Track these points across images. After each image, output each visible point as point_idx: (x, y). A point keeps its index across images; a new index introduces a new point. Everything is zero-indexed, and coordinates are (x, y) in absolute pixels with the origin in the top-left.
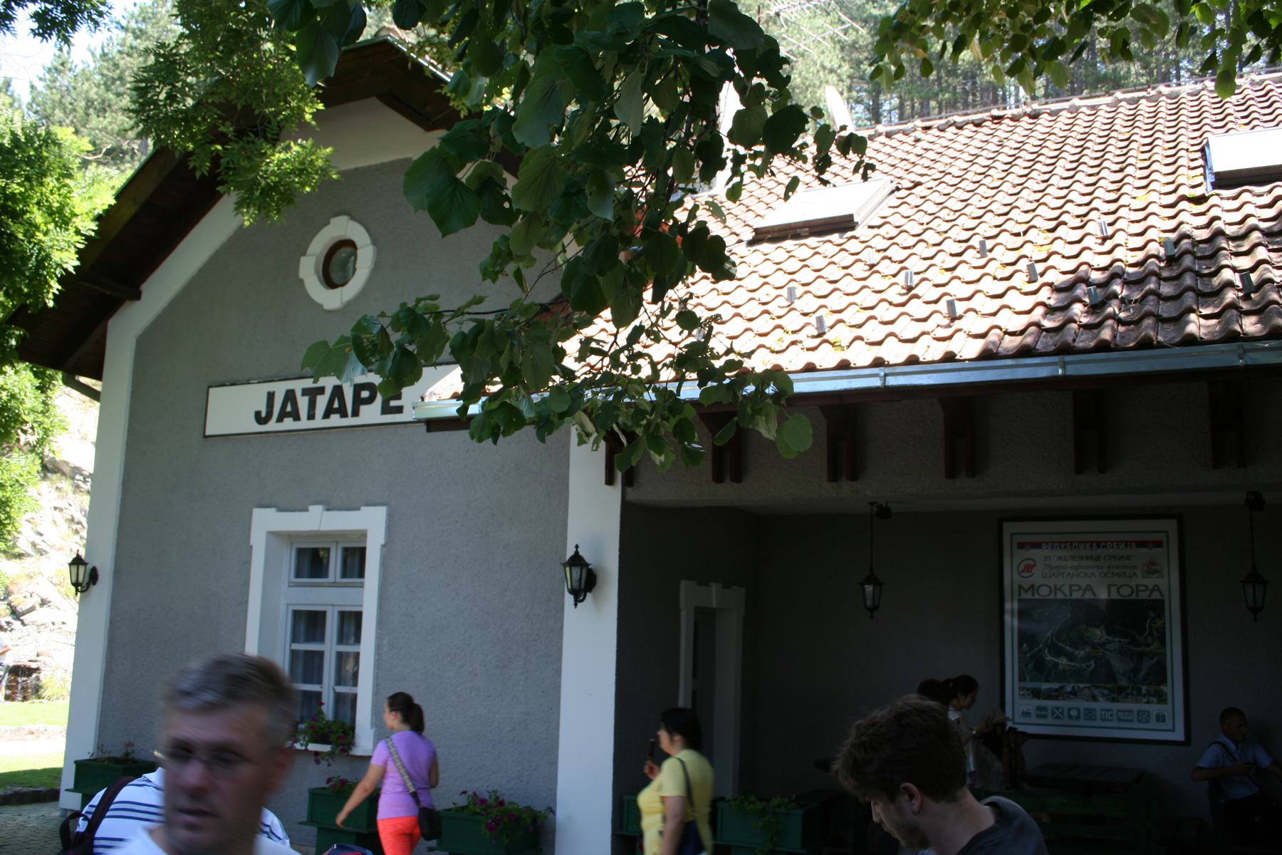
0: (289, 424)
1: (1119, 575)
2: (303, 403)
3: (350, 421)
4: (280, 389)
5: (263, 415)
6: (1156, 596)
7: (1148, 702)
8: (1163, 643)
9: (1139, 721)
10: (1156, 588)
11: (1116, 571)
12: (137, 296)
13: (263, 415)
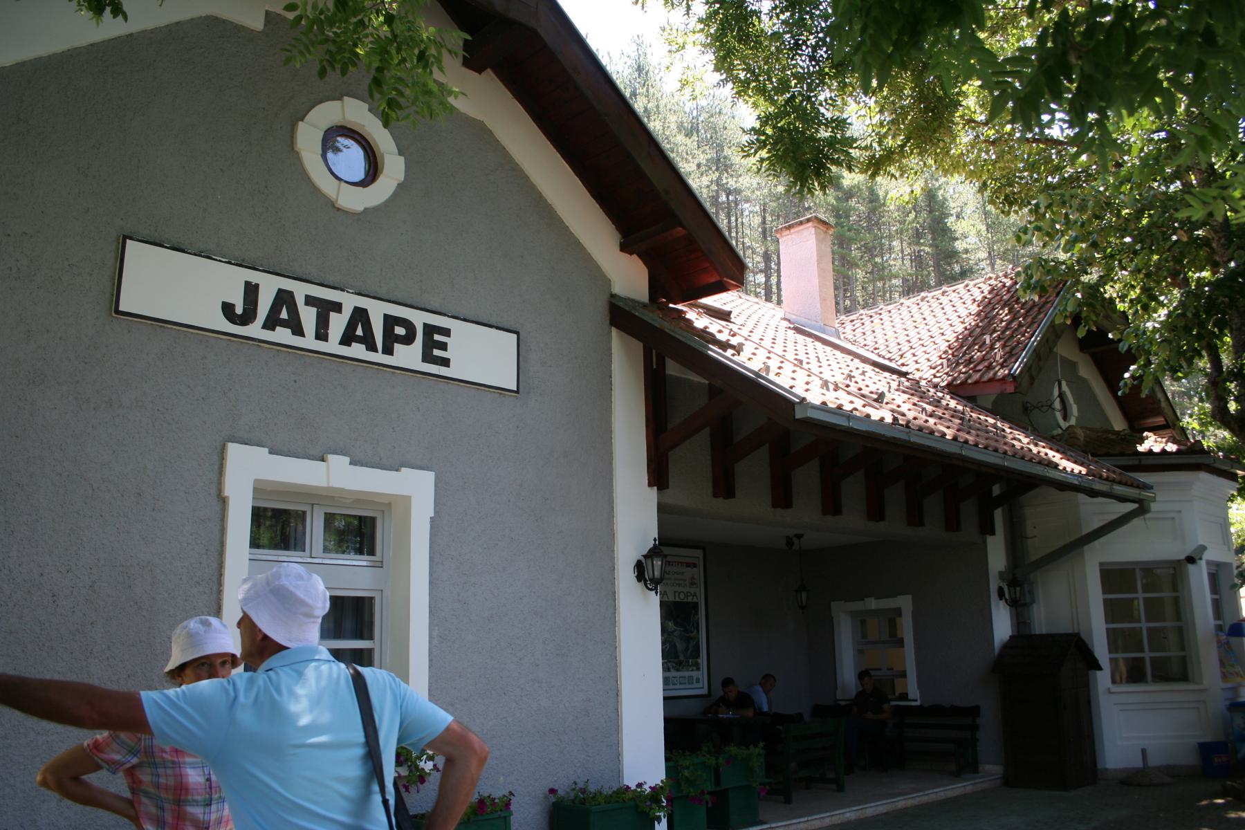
0: (283, 335)
1: (679, 585)
2: (308, 317)
3: (379, 357)
4: (269, 287)
5: (239, 310)
6: (695, 600)
7: (692, 670)
8: (698, 631)
9: (689, 684)
10: (695, 595)
11: (677, 582)
12: (625, 248)
13: (239, 310)
